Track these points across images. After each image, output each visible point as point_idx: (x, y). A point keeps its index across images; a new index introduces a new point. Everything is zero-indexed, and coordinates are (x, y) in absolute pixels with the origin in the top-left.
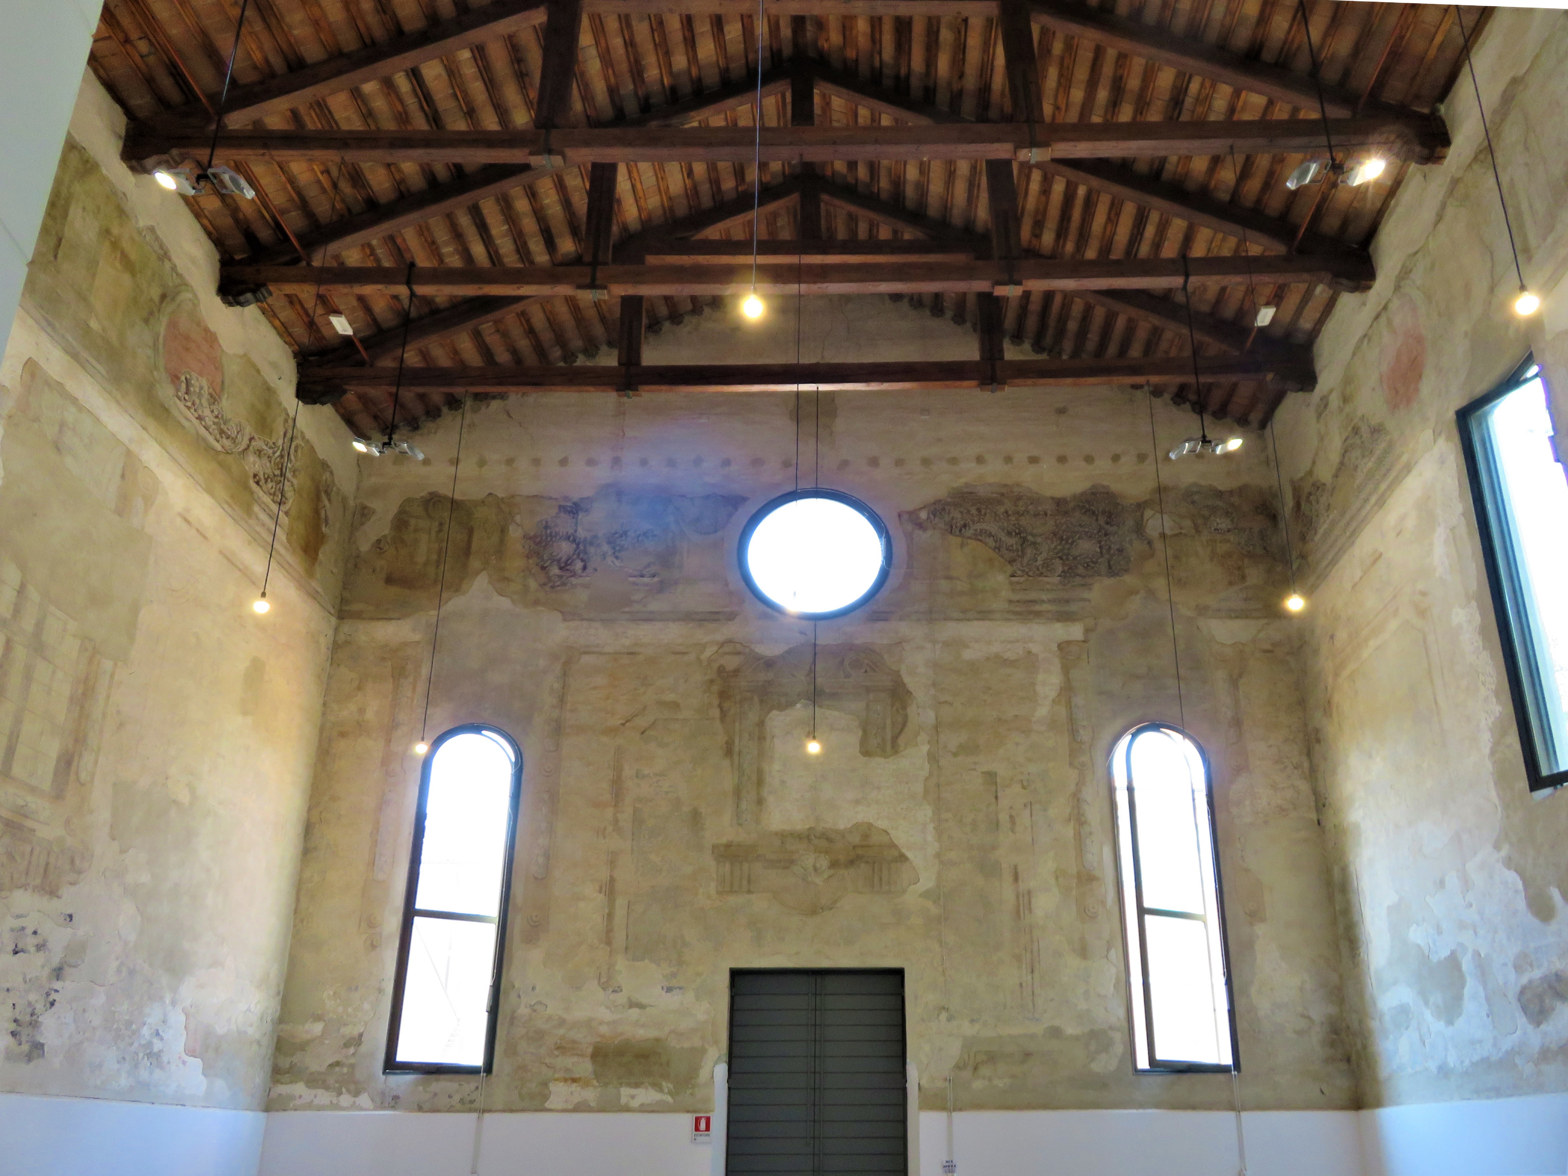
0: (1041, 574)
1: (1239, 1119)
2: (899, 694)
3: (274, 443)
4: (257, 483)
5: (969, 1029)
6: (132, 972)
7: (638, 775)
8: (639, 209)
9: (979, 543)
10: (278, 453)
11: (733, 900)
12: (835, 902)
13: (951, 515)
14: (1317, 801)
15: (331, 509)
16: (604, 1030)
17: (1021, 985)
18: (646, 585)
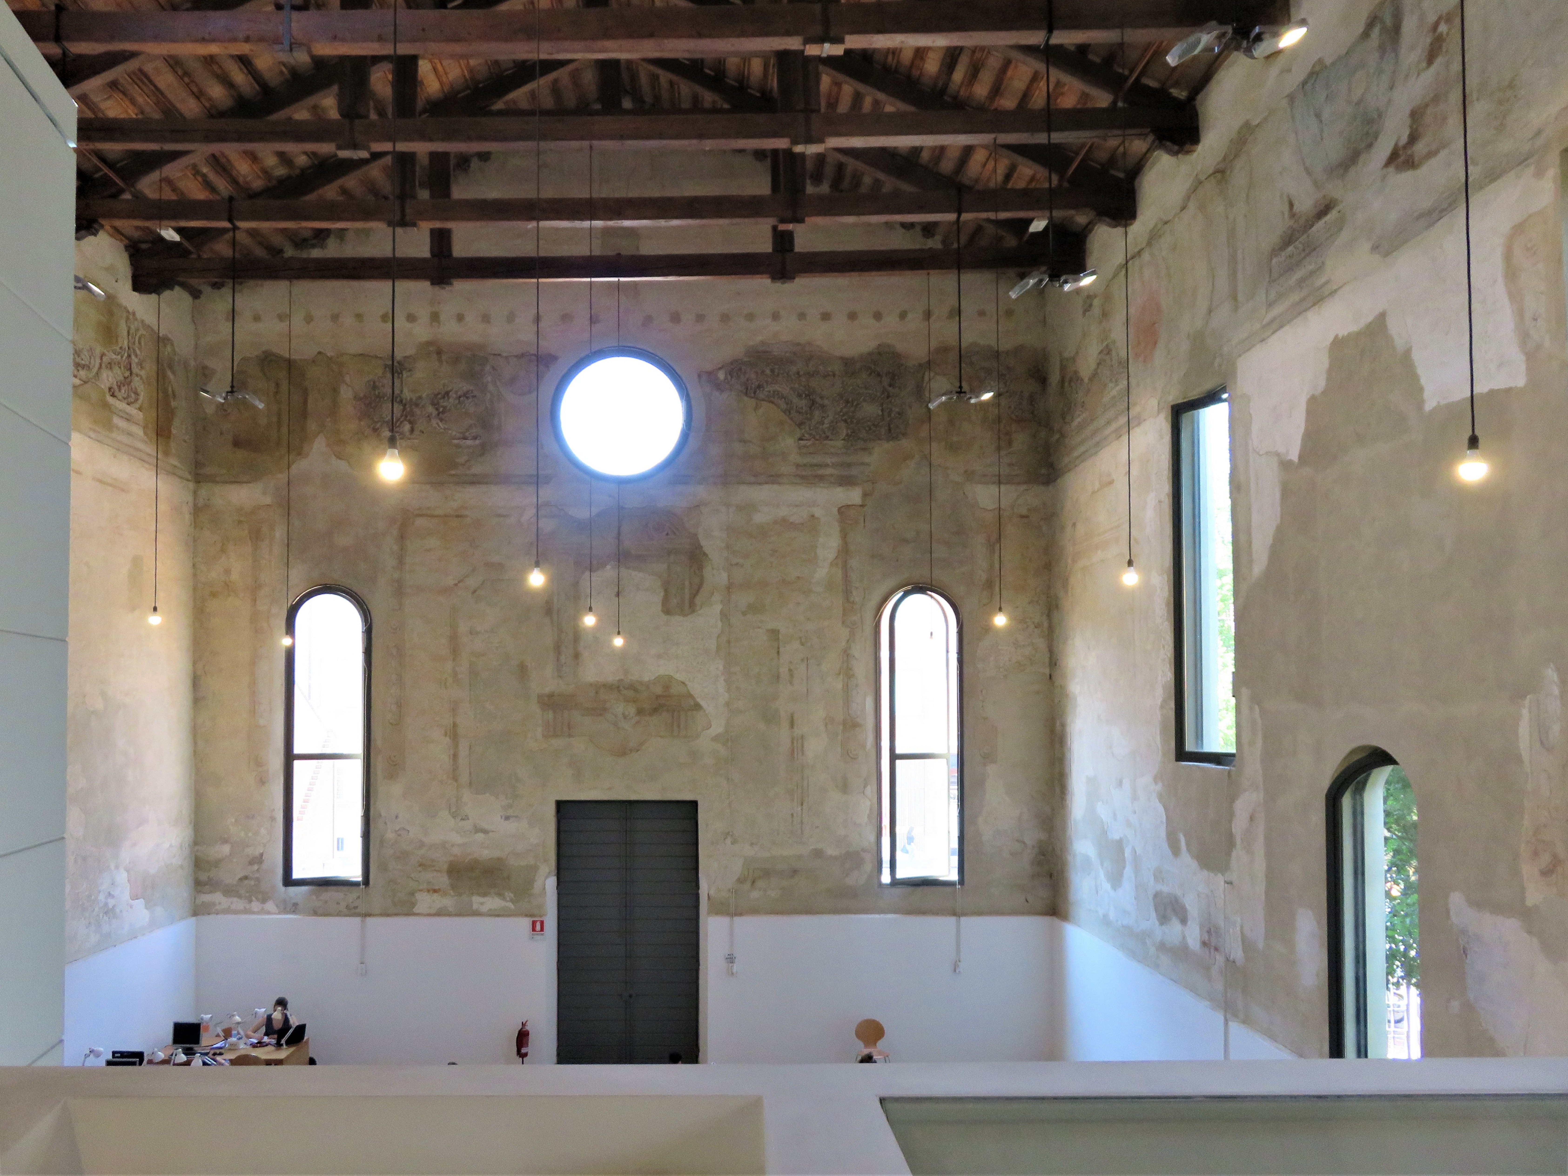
0: (827, 438)
1: (958, 922)
2: (696, 557)
3: (121, 348)
4: (113, 395)
5: (749, 851)
6: (84, 859)
7: (472, 632)
8: (441, 83)
9: (771, 404)
10: (126, 355)
11: (557, 743)
12: (641, 744)
13: (747, 376)
14: (1051, 658)
15: (175, 381)
16: (456, 851)
17: (792, 815)
18: (469, 447)
